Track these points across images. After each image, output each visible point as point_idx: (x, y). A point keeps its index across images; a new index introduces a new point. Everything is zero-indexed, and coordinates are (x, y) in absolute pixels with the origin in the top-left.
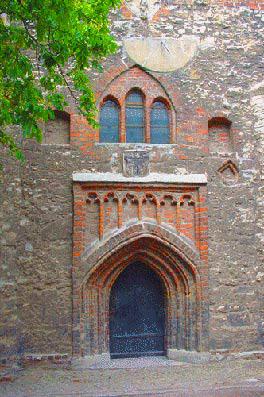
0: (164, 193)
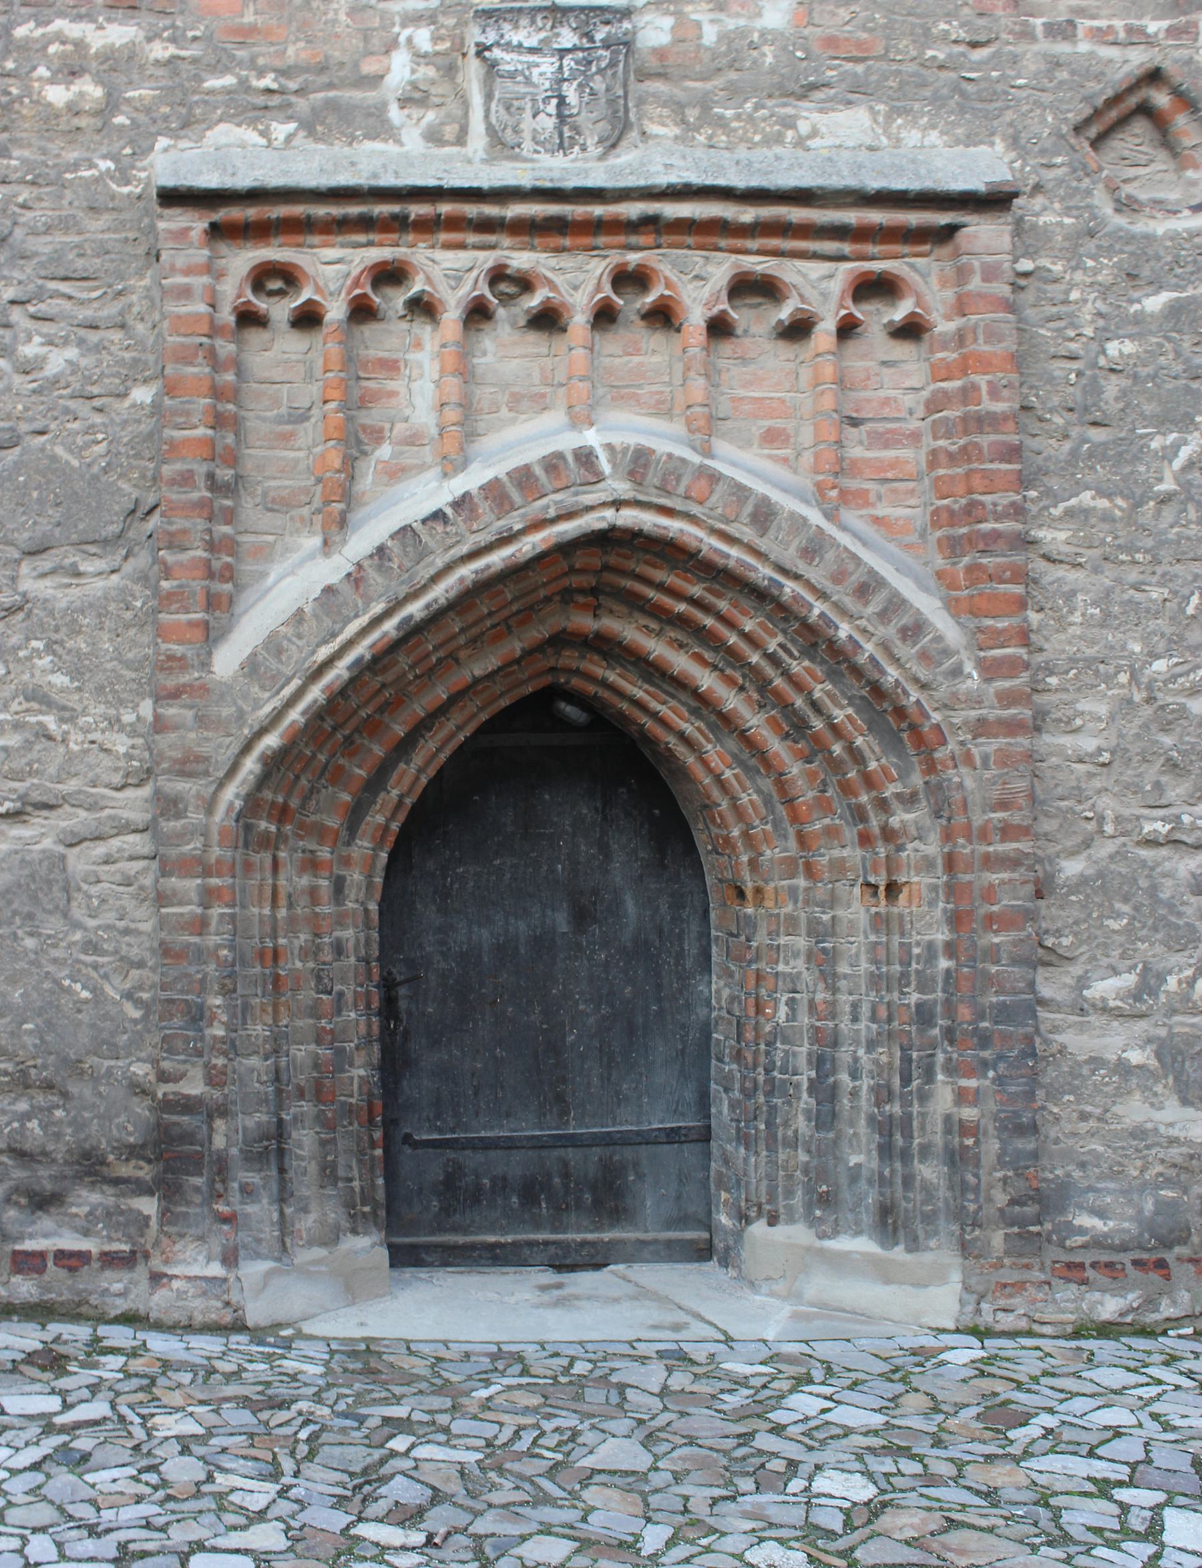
0: (721, 268)
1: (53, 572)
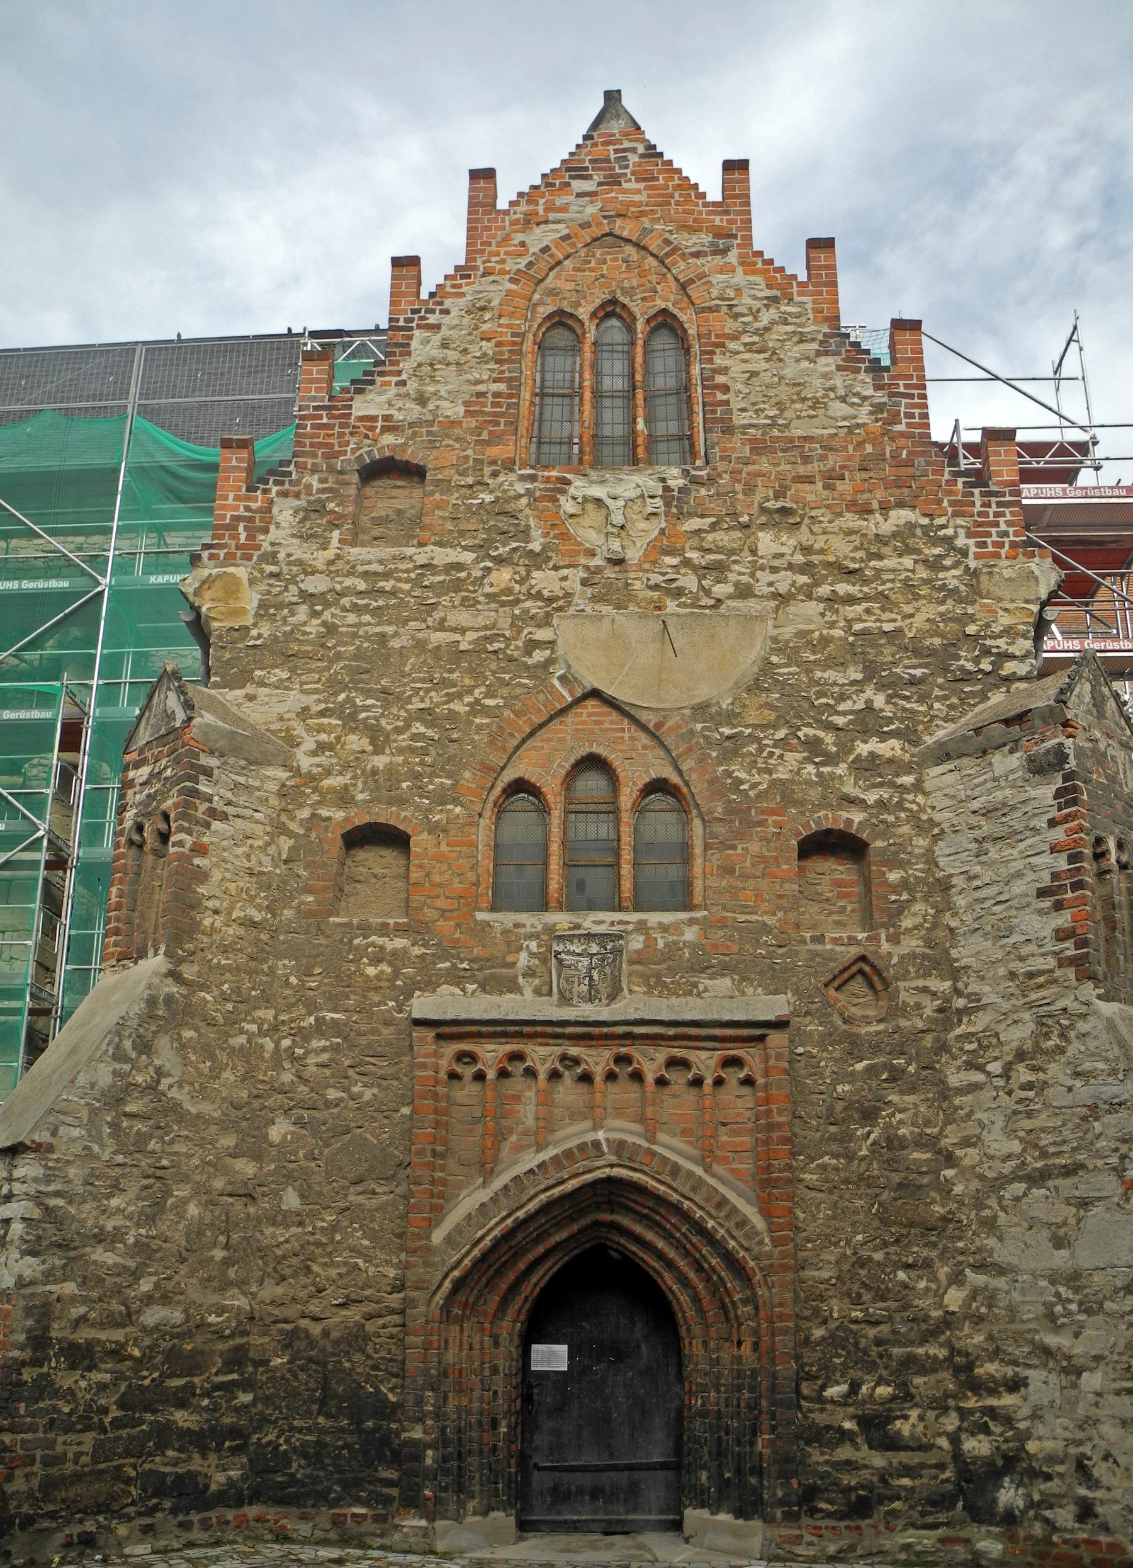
0: (661, 1054)
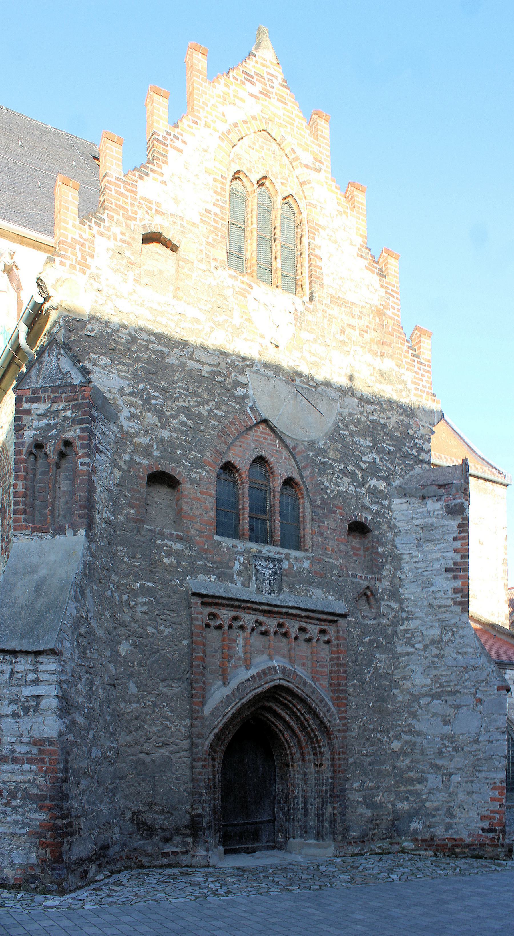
1: (167, 686)
